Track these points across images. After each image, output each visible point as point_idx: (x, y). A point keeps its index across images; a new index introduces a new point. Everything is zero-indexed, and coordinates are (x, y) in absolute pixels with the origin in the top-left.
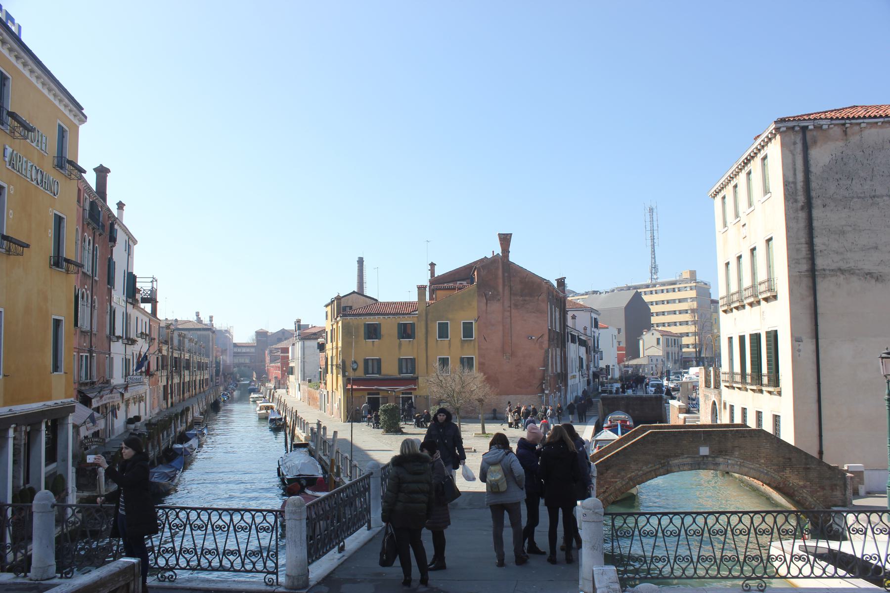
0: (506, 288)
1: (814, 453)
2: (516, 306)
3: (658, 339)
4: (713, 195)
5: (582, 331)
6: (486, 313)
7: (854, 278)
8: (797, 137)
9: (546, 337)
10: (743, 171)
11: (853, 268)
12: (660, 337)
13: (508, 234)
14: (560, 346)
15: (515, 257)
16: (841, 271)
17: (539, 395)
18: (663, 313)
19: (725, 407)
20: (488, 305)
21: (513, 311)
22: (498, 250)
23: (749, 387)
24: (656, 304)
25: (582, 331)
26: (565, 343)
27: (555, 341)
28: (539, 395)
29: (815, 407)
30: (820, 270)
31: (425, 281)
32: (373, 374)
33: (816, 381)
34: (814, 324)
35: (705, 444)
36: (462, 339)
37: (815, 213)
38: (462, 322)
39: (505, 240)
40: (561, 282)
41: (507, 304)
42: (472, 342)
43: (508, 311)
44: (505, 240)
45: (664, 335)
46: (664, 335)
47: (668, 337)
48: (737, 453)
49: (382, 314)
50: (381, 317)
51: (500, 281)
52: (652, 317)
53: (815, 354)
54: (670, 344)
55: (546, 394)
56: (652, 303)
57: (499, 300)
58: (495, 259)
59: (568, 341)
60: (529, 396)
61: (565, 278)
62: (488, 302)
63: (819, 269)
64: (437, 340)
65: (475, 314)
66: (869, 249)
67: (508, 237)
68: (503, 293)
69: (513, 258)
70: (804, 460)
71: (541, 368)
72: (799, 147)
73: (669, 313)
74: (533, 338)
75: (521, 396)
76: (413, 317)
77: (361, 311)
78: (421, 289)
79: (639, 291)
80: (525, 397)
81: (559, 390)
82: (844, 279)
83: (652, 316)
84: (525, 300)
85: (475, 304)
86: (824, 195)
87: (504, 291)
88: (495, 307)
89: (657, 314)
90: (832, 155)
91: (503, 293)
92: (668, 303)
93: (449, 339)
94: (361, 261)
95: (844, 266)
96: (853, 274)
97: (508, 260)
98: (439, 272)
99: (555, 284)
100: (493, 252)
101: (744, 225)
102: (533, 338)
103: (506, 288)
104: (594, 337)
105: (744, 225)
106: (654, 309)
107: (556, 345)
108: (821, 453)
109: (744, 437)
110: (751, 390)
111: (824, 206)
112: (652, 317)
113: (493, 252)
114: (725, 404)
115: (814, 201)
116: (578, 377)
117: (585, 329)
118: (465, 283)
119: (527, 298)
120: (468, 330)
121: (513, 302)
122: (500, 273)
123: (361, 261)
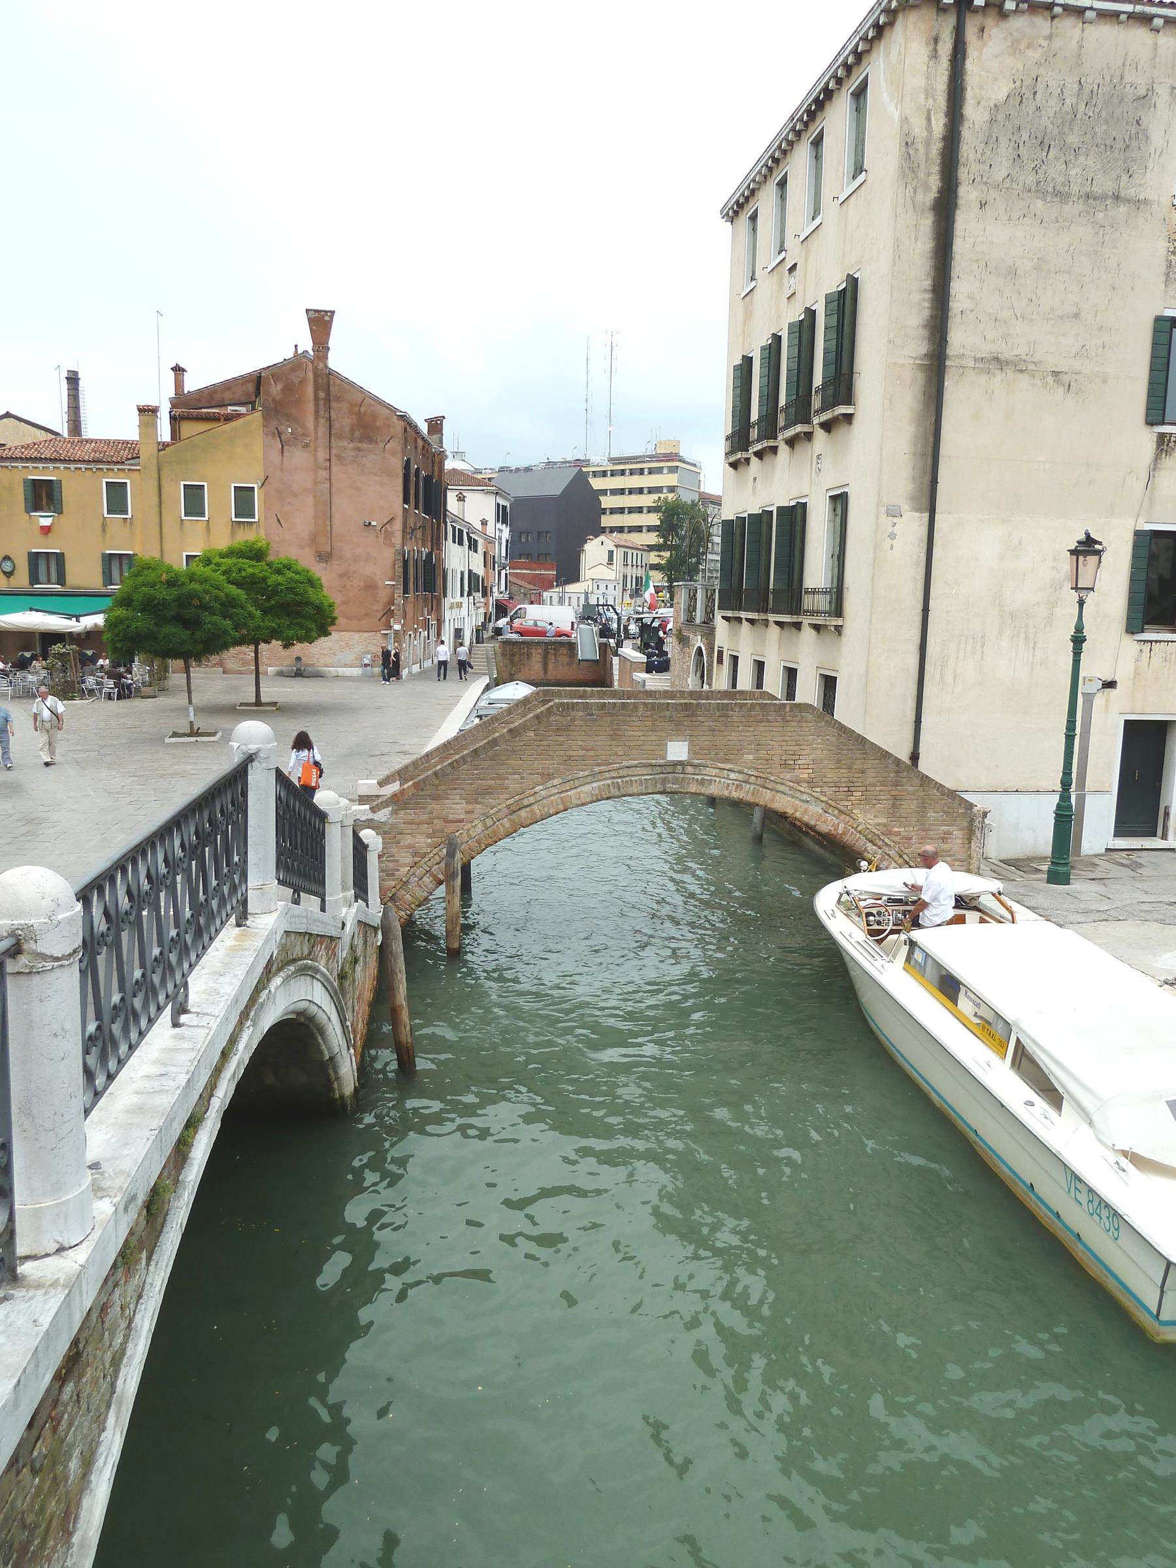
0: (322, 421)
1: (904, 755)
2: (339, 457)
3: (611, 553)
4: (731, 213)
5: (479, 527)
6: (282, 470)
7: (1024, 381)
8: (944, 24)
9: (398, 526)
10: (804, 137)
11: (1024, 357)
12: (614, 549)
13: (326, 312)
14: (429, 543)
15: (339, 361)
16: (999, 362)
17: (383, 632)
18: (621, 511)
19: (720, 661)
20: (286, 453)
21: (334, 468)
22: (306, 344)
23: (772, 617)
24: (612, 475)
25: (479, 527)
26: (438, 538)
27: (419, 533)
28: (383, 632)
29: (158, 528)
30: (956, 356)
31: (162, 397)
32: (49, 582)
33: (920, 606)
34: (928, 478)
35: (677, 734)
36: (234, 519)
37: (965, 222)
38: (233, 485)
39: (320, 323)
40: (436, 425)
41: (322, 454)
42: (255, 526)
43: (326, 469)
44: (320, 323)
45: (620, 546)
46: (620, 546)
47: (626, 550)
48: (751, 757)
49: (64, 461)
50: (62, 466)
51: (310, 407)
52: (602, 516)
53: (924, 545)
54: (629, 562)
55: (396, 632)
56: (604, 492)
57: (306, 446)
58: (296, 363)
59: (446, 539)
60: (365, 635)
61: (444, 417)
62: (285, 447)
63: (956, 353)
64: (182, 520)
65: (259, 471)
66: (1062, 317)
67: (327, 318)
68: (316, 433)
69: (335, 362)
70: (892, 775)
71: (387, 583)
72: (946, 47)
73: (632, 510)
74: (374, 523)
75: (347, 634)
76: (129, 470)
77: (18, 454)
78: (147, 412)
79: (584, 470)
80: (356, 636)
81: (426, 625)
82: (1002, 381)
83: (604, 513)
84: (359, 449)
85: (258, 449)
86: (985, 179)
87: (316, 427)
88: (298, 457)
89: (613, 511)
90: (1015, 83)
91: (316, 433)
92: (630, 493)
93: (206, 518)
94: (73, 380)
95: (1006, 353)
96: (1021, 371)
97: (326, 367)
98: (192, 384)
99: (424, 428)
100: (296, 346)
101: (793, 268)
102: (374, 523)
103: (322, 421)
104: (500, 538)
105: (793, 268)
106: (607, 502)
107: (420, 542)
108: (915, 757)
109: (768, 721)
110: (777, 623)
111: (983, 205)
112: (602, 516)
113: (296, 346)
114: (720, 653)
115: (962, 191)
116: (465, 606)
117: (484, 523)
118: (242, 410)
119: (364, 446)
120: (244, 497)
121: (334, 451)
122: (310, 390)
123: (73, 380)
